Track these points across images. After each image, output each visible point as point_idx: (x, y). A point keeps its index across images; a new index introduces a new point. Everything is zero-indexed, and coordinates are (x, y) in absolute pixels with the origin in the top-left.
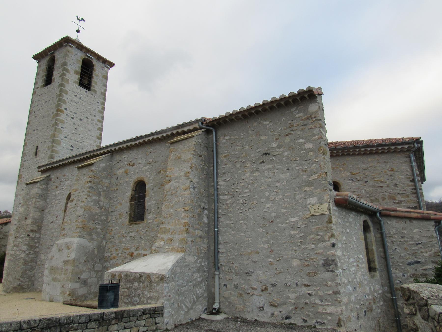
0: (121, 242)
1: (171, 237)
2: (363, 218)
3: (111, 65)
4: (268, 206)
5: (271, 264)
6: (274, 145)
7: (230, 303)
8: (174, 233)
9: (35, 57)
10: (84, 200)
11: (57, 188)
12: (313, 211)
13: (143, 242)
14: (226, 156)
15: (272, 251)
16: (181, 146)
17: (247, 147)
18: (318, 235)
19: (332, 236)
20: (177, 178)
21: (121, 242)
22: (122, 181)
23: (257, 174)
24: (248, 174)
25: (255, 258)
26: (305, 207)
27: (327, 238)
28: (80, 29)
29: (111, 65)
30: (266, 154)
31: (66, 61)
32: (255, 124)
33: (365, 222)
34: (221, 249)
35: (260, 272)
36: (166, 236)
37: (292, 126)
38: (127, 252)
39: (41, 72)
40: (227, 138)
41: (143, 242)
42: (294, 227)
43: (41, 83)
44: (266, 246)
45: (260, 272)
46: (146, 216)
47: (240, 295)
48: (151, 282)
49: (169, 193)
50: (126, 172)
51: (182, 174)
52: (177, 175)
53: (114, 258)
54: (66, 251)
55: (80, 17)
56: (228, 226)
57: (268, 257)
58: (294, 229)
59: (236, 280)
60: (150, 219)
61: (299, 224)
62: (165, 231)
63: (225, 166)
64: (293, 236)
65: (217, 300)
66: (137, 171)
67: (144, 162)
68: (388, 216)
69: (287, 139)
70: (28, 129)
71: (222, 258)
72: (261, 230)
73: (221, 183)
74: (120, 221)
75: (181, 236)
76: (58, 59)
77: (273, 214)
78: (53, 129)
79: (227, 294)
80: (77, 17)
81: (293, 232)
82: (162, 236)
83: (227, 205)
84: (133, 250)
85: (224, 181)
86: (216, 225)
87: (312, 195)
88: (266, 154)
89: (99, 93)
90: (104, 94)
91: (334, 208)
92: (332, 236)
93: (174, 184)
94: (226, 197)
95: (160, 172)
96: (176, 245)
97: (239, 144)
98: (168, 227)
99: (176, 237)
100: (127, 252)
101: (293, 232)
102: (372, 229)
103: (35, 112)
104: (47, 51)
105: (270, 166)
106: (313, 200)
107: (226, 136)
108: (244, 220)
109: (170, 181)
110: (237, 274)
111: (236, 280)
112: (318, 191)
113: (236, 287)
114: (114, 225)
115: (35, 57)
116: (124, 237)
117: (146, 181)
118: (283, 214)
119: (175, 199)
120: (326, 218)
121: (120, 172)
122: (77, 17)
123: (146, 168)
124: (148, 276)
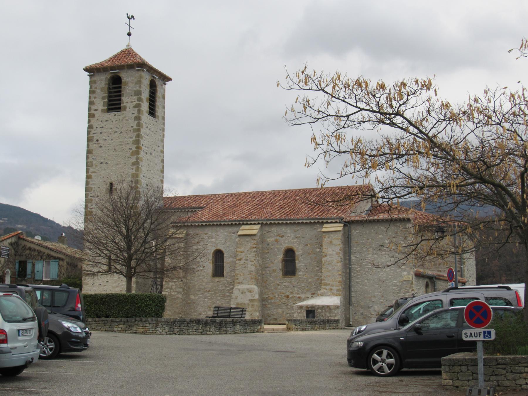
0: (276, 288)
1: (331, 287)
2: (426, 280)
3: (169, 79)
4: (381, 273)
5: (382, 302)
6: (387, 242)
7: (358, 322)
8: (332, 286)
9: (86, 70)
10: (252, 260)
11: (198, 243)
12: (405, 278)
13: (296, 289)
14: (356, 243)
15: (383, 296)
16: (332, 235)
17: (370, 240)
18: (103, 253)
19: (413, 290)
20: (331, 255)
21: (276, 288)
22: (273, 247)
23: (376, 256)
24: (371, 255)
25: (373, 299)
26: (401, 276)
27: (410, 291)
28: (132, 31)
29: (169, 79)
30: (382, 246)
31: (141, 89)
32: (376, 227)
33: (427, 282)
34: (353, 294)
35: (375, 306)
36: (328, 287)
37: (397, 233)
38: (283, 295)
39: (98, 91)
40: (357, 231)
41: (296, 289)
42: (395, 285)
43: (100, 104)
44: (379, 294)
45: (375, 306)
46: (297, 273)
47: (364, 318)
48: (330, 309)
49: (327, 263)
50: (277, 241)
51: (334, 253)
52: (331, 253)
53: (272, 299)
54: (248, 294)
55: (130, 15)
56: (357, 282)
57: (380, 299)
58: (395, 286)
59: (362, 310)
60: (301, 275)
61: (398, 284)
62: (326, 285)
63: (355, 248)
64: (394, 290)
65: (351, 320)
66: (287, 241)
67: (293, 236)
68: (439, 279)
69: (394, 240)
70: (90, 160)
71: (353, 299)
72: (377, 286)
73: (352, 258)
74: (273, 274)
75: (337, 288)
76: (126, 83)
77: (384, 278)
78: (134, 167)
79: (356, 318)
80: (127, 14)
81: (394, 288)
82: (324, 287)
83: (357, 271)
84: (288, 294)
85: (355, 257)
86: (350, 282)
87: (405, 270)
88: (382, 246)
89: (160, 118)
90: (163, 118)
91: (414, 277)
92: (413, 290)
93: (328, 258)
94: (356, 266)
95: (307, 245)
96: (335, 292)
97: (366, 236)
98: (328, 282)
99: (335, 288)
100: (283, 295)
101: (394, 288)
102: (430, 286)
103: (97, 141)
104: (109, 68)
105: (384, 253)
106: (405, 273)
107: (356, 230)
108: (367, 280)
109: (326, 256)
110: (362, 307)
111: (362, 310)
112: (408, 269)
113: (362, 314)
114: (269, 277)
115: (86, 70)
116: (278, 285)
117: (295, 249)
118: (390, 278)
119: (330, 268)
120: (411, 282)
121: (270, 240)
122: (127, 14)
123: (295, 240)
124: (328, 306)
